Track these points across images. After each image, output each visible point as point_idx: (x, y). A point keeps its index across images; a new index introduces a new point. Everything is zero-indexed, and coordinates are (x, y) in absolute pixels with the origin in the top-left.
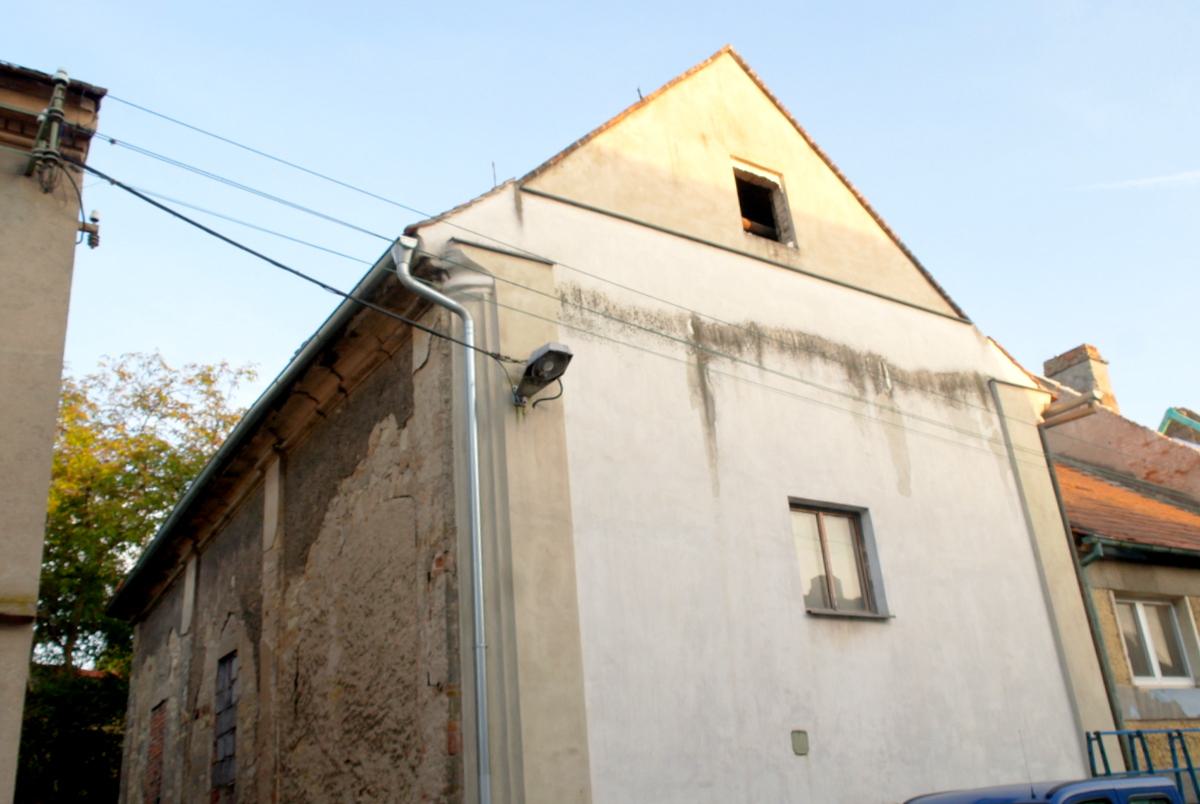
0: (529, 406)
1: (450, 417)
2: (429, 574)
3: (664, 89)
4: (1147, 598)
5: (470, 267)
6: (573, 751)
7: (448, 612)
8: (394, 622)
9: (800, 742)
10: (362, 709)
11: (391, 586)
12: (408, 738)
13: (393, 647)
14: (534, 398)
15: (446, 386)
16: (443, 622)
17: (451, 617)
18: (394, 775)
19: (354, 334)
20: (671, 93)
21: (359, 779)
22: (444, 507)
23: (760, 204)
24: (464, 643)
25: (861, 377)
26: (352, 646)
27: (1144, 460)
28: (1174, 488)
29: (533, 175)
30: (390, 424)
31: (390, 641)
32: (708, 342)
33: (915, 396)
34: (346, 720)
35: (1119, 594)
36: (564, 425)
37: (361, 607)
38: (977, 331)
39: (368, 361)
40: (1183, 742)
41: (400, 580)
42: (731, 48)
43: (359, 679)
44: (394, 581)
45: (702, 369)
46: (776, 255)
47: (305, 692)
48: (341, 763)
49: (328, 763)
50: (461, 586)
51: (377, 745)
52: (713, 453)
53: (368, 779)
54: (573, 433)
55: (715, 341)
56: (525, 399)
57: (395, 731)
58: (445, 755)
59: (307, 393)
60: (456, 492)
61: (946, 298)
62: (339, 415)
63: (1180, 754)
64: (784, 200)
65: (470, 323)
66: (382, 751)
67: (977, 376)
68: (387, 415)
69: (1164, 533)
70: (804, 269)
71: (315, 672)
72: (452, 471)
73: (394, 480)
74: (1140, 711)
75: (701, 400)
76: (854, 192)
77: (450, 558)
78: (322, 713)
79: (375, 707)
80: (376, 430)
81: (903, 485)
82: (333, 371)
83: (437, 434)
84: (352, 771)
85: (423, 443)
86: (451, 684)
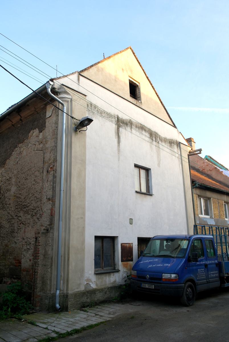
0: (78, 132)
1: (57, 131)
2: (48, 171)
3: (115, 54)
4: (203, 197)
5: (66, 92)
6: (82, 218)
7: (53, 181)
8: (35, 182)
9: (131, 221)
10: (22, 203)
11: (34, 173)
12: (37, 211)
13: (34, 188)
14: (80, 130)
15: (57, 123)
16: (52, 183)
17: (54, 182)
18: (32, 220)
19: (28, 105)
20: (116, 56)
21: (20, 220)
22: (54, 154)
23: (134, 90)
24: (57, 189)
25: (153, 137)
26: (20, 187)
27: (202, 166)
28: (208, 174)
29: (82, 71)
30: (36, 131)
31: (33, 186)
32: (120, 123)
33: (163, 144)
34: (17, 205)
35: (199, 196)
36: (86, 138)
37: (24, 177)
38: (178, 130)
39: (31, 113)
40: (212, 229)
41: (37, 172)
42: (131, 47)
43: (22, 196)
44: (35, 172)
45: (118, 129)
46: (137, 103)
47: (3, 197)
48: (14, 216)
49: (9, 216)
50: (58, 175)
51: (27, 212)
52: (119, 150)
53: (23, 221)
54: (88, 140)
55: (122, 123)
56: (77, 130)
57: (33, 209)
58: (49, 216)
59: (10, 119)
60: (58, 151)
61: (172, 121)
62: (19, 126)
63: (211, 231)
64: (139, 90)
65: (65, 108)
66: (28, 214)
67: (177, 141)
68: (36, 129)
69: (206, 183)
70: (142, 108)
71: (6, 193)
72: (57, 145)
73: (37, 146)
74: (199, 222)
75: (117, 137)
76: (155, 91)
77: (55, 167)
78: (8, 203)
79: (27, 203)
80: (32, 132)
81: (159, 165)
82: (19, 114)
83: (53, 135)
84: (18, 218)
85: (49, 137)
86: (53, 199)
